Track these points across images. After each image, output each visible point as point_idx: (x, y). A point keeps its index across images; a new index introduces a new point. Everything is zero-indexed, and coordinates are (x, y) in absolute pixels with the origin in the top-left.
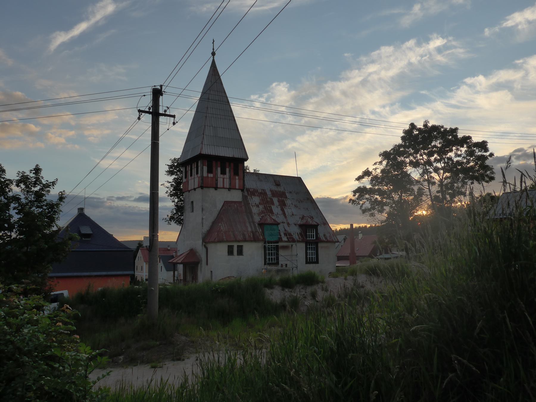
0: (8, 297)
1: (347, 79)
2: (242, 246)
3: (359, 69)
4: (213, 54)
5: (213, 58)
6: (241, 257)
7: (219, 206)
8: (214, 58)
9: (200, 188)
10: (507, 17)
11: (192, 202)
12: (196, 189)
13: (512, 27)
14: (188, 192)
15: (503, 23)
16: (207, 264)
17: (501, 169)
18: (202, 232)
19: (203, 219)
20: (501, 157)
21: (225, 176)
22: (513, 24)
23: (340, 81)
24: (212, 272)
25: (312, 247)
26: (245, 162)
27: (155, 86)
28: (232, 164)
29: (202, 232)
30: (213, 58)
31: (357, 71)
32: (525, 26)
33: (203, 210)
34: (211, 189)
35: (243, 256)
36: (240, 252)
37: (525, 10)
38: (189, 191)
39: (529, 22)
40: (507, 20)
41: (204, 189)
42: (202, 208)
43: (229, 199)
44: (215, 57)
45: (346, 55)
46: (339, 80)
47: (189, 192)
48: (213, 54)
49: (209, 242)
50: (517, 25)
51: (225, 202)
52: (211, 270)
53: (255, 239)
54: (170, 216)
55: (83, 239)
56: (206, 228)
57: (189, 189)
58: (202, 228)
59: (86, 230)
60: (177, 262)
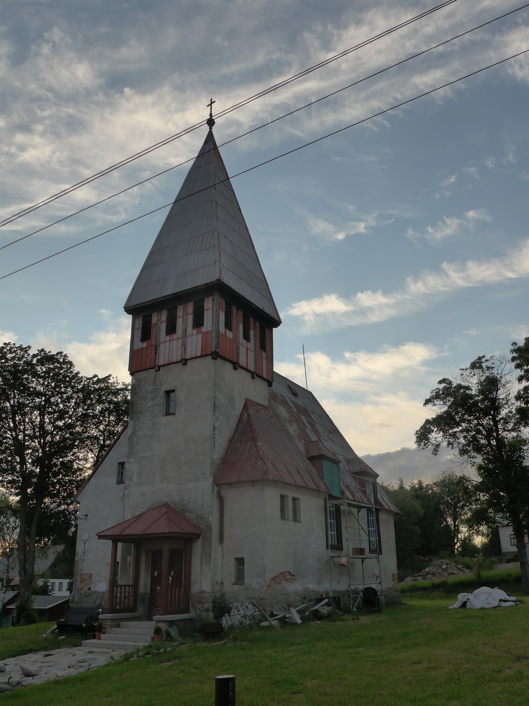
0: (328, 494)
1: (99, 343)
3: (117, 333)
5: (211, 128)
9: (210, 357)
10: (294, 305)
12: (161, 369)
13: (299, 316)
14: (152, 371)
15: (289, 310)
16: (221, 540)
19: (214, 428)
20: (383, 454)
21: (249, 344)
22: (300, 313)
23: (89, 344)
24: (240, 562)
30: (211, 128)
31: (114, 335)
32: (312, 318)
37: (313, 300)
39: (317, 315)
40: (295, 308)
42: (214, 402)
43: (253, 397)
45: (103, 311)
46: (89, 342)
50: (304, 315)
56: (219, 453)
57: (161, 363)
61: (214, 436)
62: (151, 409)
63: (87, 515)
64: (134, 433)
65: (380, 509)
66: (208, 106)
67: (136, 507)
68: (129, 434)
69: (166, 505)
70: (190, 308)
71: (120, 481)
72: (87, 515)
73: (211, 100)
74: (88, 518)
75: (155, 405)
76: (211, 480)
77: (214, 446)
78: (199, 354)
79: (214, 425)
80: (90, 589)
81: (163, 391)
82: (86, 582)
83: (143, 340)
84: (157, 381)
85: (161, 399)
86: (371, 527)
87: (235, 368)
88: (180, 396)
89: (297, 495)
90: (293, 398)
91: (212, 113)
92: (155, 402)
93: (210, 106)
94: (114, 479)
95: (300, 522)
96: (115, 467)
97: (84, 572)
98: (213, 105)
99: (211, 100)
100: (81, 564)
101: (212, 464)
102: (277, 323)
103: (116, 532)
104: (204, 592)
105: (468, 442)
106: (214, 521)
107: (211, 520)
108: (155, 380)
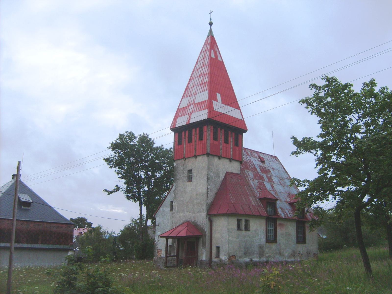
2: (249, 220)
4: (211, 24)
5: (211, 27)
6: (248, 232)
7: (222, 176)
8: (212, 28)
11: (190, 171)
12: (186, 159)
14: (183, 160)
17: (16, 166)
18: (207, 203)
19: (208, 189)
21: (228, 145)
25: (271, 235)
26: (244, 133)
27: (325, 74)
28: (233, 134)
29: (207, 203)
30: (211, 27)
33: (208, 179)
34: (191, 159)
35: (249, 232)
36: (247, 228)
38: (185, 159)
41: (210, 156)
42: (208, 177)
43: (230, 170)
44: (212, 26)
47: (185, 160)
48: (211, 24)
49: (218, 215)
51: (227, 173)
52: (218, 246)
53: (259, 216)
54: (330, 176)
55: (23, 207)
56: (211, 199)
58: (207, 199)
59: (25, 198)
60: (169, 236)
61: (207, 193)
62: (182, 178)
63: (159, 224)
64: (176, 189)
65: (306, 221)
66: (210, 14)
67: (177, 222)
68: (174, 190)
69: (188, 222)
70: (198, 129)
71: (171, 210)
72: (159, 224)
73: (211, 11)
74: (159, 225)
75: (184, 176)
76: (206, 213)
77: (208, 197)
78: (201, 154)
79: (208, 187)
80: (161, 256)
81: (187, 170)
82: (159, 253)
83: (178, 145)
84: (185, 165)
85: (186, 174)
86: (269, 235)
87: (220, 159)
88: (194, 174)
89: (247, 219)
90: (260, 163)
91: (212, 18)
92: (184, 175)
93: (210, 14)
94: (169, 209)
95: (249, 231)
96: (170, 203)
97: (159, 248)
98: (212, 13)
99: (211, 11)
100: (157, 245)
101: (206, 205)
102: (245, 131)
103: (166, 235)
104: (203, 260)
105: (133, 257)
106: (207, 230)
107: (206, 230)
108: (184, 164)
